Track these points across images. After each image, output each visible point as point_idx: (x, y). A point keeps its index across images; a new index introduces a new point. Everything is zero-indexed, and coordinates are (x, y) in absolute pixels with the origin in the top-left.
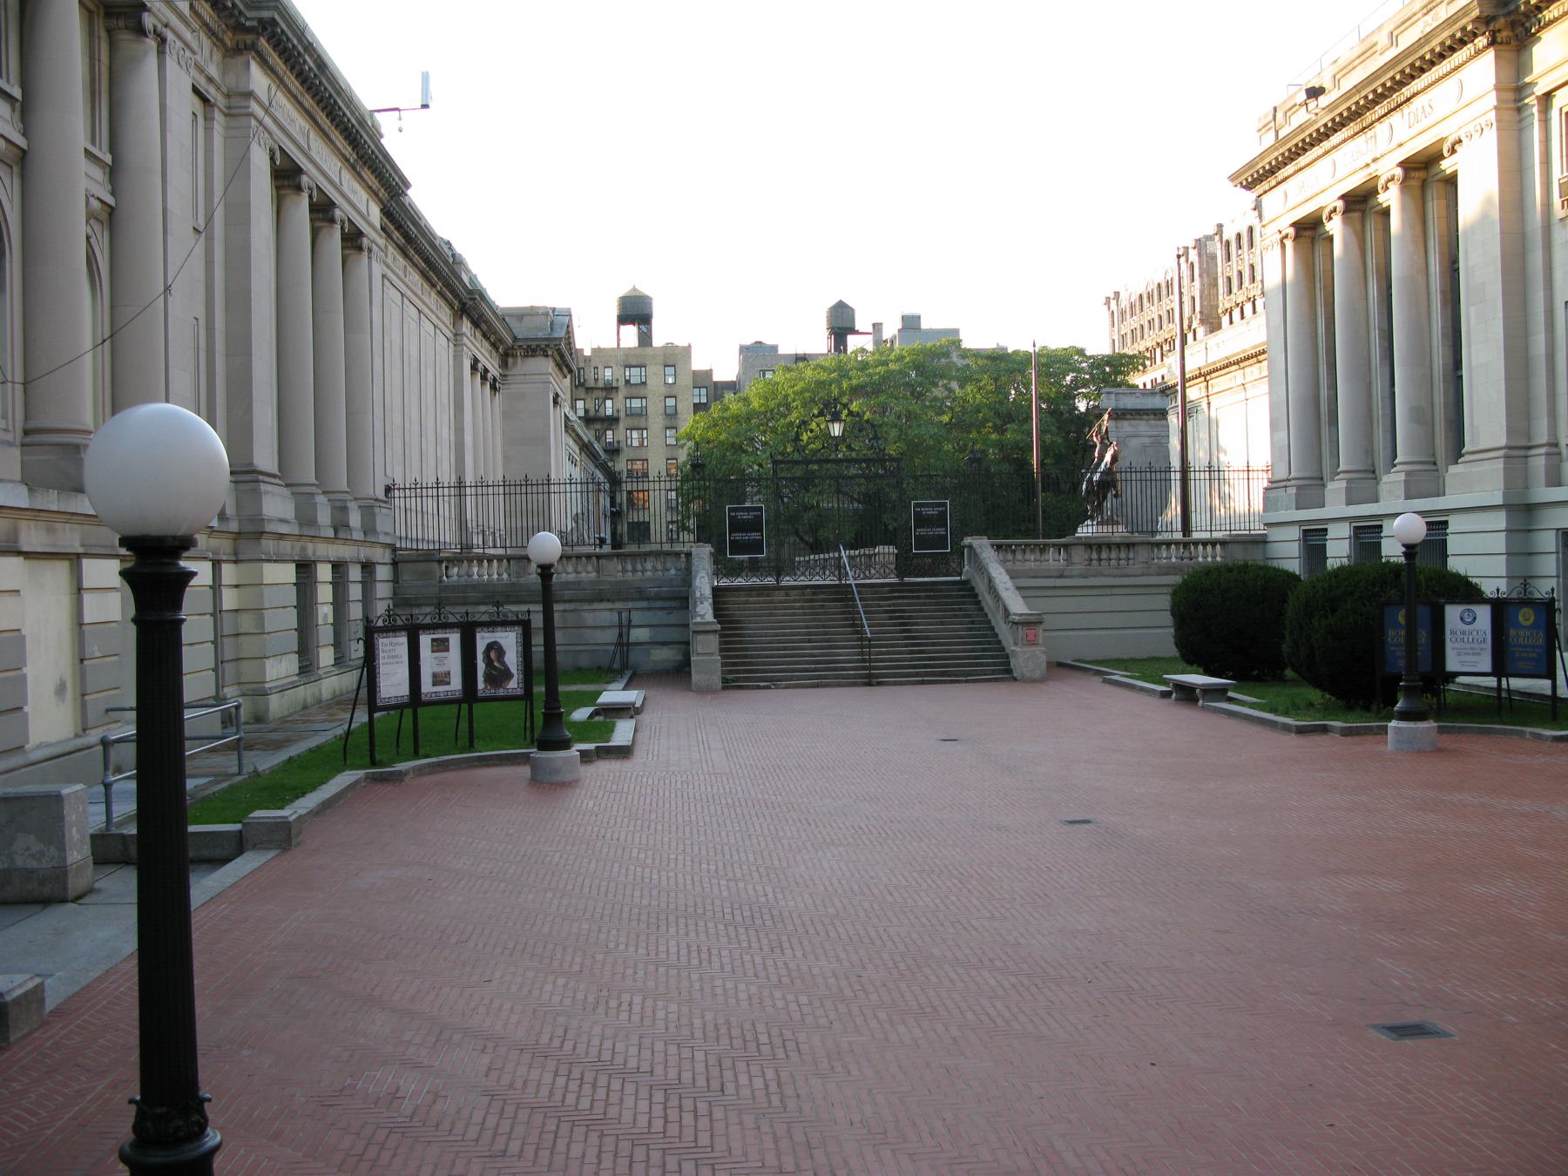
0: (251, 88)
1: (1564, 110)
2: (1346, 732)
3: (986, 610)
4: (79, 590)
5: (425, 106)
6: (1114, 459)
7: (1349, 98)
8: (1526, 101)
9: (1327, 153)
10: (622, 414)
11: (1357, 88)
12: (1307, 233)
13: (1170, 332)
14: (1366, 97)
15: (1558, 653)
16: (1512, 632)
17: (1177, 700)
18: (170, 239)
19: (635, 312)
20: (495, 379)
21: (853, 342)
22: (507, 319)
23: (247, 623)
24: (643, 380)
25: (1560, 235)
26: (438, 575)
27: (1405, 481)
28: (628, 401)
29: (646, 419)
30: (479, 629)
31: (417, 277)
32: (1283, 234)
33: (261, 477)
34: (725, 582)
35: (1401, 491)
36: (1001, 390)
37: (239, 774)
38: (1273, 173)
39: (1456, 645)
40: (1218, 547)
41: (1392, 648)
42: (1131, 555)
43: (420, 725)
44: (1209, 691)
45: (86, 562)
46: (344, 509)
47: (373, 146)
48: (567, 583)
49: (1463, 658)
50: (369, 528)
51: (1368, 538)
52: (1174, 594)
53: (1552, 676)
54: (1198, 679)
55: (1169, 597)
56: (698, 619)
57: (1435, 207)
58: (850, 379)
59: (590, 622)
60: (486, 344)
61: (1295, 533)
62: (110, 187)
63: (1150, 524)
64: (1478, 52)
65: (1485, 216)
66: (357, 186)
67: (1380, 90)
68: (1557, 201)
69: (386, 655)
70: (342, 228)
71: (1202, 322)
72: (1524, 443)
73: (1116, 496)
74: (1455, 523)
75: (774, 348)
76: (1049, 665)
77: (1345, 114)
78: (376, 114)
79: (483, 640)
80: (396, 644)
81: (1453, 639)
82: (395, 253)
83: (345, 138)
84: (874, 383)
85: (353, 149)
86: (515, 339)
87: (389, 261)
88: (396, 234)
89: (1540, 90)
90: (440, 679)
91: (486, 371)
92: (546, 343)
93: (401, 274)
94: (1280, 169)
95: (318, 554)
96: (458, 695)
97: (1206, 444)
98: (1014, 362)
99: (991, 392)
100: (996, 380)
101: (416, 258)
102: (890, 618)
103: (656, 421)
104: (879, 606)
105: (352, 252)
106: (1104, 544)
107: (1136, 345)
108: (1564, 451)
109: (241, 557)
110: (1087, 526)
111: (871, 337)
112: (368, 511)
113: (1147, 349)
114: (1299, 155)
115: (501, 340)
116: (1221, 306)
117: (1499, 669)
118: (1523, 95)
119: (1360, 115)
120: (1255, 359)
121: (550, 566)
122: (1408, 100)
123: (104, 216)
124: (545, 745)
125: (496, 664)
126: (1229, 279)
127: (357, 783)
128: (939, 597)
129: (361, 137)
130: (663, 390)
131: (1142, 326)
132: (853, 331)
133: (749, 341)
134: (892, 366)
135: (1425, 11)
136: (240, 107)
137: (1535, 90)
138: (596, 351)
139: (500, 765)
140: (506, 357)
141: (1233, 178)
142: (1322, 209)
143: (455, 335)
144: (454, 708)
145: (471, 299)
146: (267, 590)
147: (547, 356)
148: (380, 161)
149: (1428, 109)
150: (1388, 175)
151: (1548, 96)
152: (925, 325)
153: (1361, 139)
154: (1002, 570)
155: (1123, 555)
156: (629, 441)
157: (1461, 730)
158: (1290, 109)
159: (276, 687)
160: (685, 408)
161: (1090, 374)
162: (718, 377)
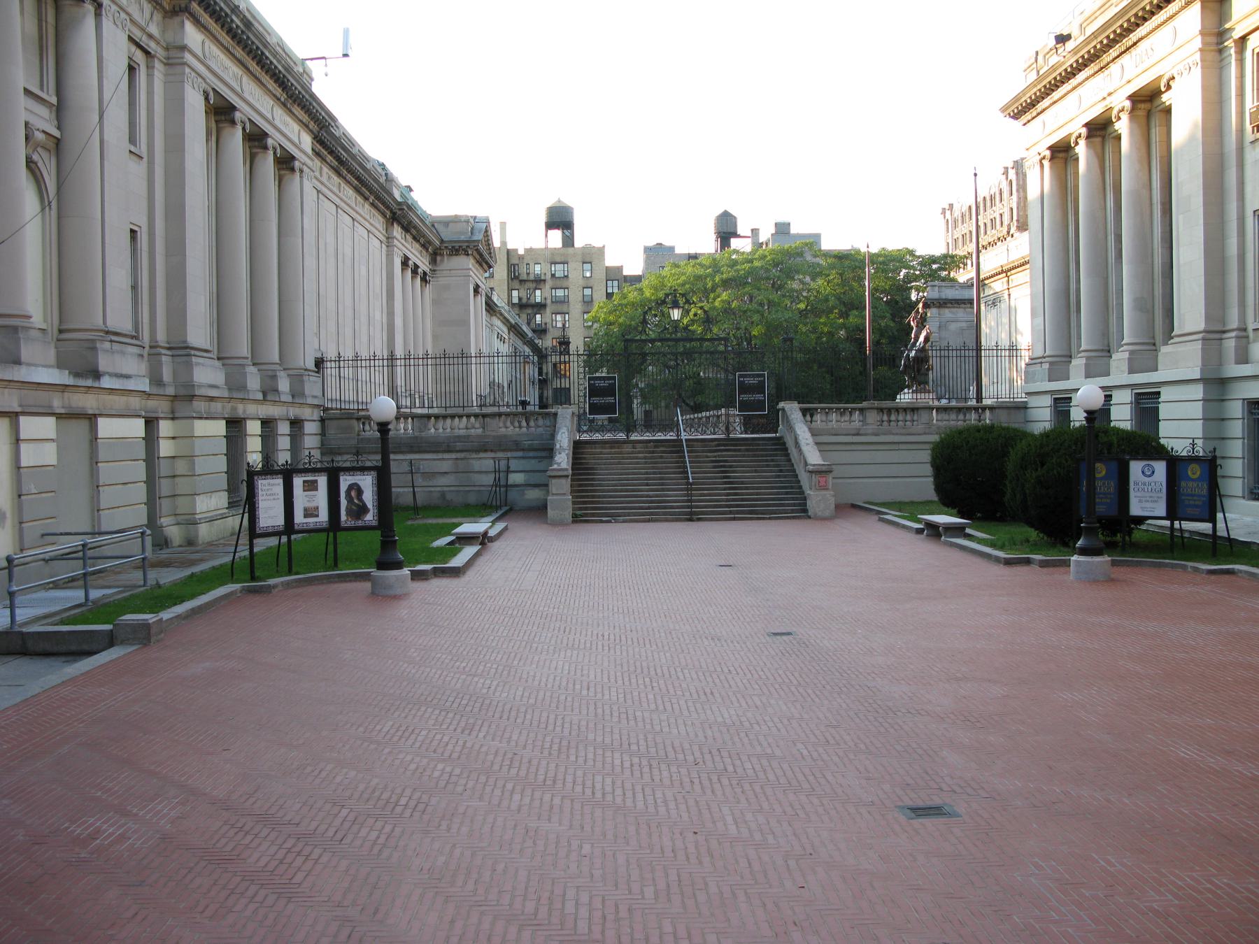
0: (185, 42)
1: (1256, 51)
2: (1043, 564)
3: (793, 461)
4: (17, 441)
5: (346, 55)
6: (927, 339)
7: (1089, 43)
8: (1226, 44)
9: (1074, 88)
10: (549, 302)
11: (1095, 35)
12: (1061, 155)
14: (1101, 42)
15: (1218, 500)
16: (1183, 484)
17: (927, 535)
18: (106, 163)
19: (560, 220)
20: (425, 273)
21: (735, 243)
22: (436, 225)
23: (181, 467)
24: (566, 274)
25: (1252, 155)
26: (357, 429)
27: (1129, 359)
28: (553, 291)
29: (568, 307)
30: (342, 473)
31: (351, 192)
32: (1042, 156)
33: (193, 352)
34: (585, 437)
35: (1125, 367)
37: (144, 586)
38: (1034, 106)
39: (1139, 494)
41: (1183, 498)
42: (915, 418)
43: (339, 551)
45: (22, 419)
46: (274, 377)
47: (299, 88)
48: (459, 437)
49: (1144, 505)
50: (297, 394)
51: (1148, 404)
52: (933, 450)
53: (1213, 520)
54: (942, 519)
55: (929, 452)
56: (555, 466)
57: (1156, 133)
58: (722, 274)
59: (477, 469)
60: (418, 246)
61: (1047, 401)
62: (56, 122)
63: (963, 393)
65: (1192, 138)
66: (289, 120)
67: (1112, 36)
68: (1248, 127)
69: (264, 493)
70: (275, 153)
72: (1221, 328)
74: (1166, 394)
75: (672, 249)
77: (1086, 56)
78: (307, 62)
79: (345, 481)
80: (273, 485)
81: (1136, 489)
82: (330, 173)
83: (275, 82)
84: (741, 277)
85: (283, 90)
86: (442, 241)
87: (324, 179)
88: (329, 158)
89: (1237, 34)
90: (309, 513)
91: (416, 267)
92: (466, 244)
93: (335, 189)
94: (1039, 102)
95: (248, 413)
96: (325, 525)
97: (1007, 327)
99: (838, 285)
100: (841, 275)
101: (349, 177)
102: (715, 467)
103: (576, 307)
104: (707, 457)
105: (287, 172)
106: (893, 408)
107: (965, 247)
108: (1251, 334)
109: (177, 415)
110: (904, 394)
111: (749, 240)
112: (297, 379)
114: (1053, 91)
115: (430, 243)
117: (1172, 514)
118: (1225, 39)
119: (1098, 57)
121: (387, 424)
122: (1135, 44)
123: (51, 145)
124: (383, 565)
125: (356, 501)
127: (232, 593)
128: (757, 450)
129: (288, 80)
130: (581, 282)
132: (736, 235)
133: (651, 243)
134: (756, 264)
136: (178, 58)
138: (529, 251)
139: (355, 581)
140: (435, 256)
141: (1003, 110)
142: (1070, 135)
143: (388, 238)
144: (324, 535)
145: (400, 209)
146: (197, 442)
147: (468, 255)
148: (307, 100)
150: (1120, 107)
151: (1244, 39)
152: (793, 230)
153: (1100, 76)
155: (908, 417)
156: (554, 323)
157: (1139, 564)
158: (1048, 53)
159: (205, 518)
160: (600, 297)
161: (920, 270)
162: (627, 272)
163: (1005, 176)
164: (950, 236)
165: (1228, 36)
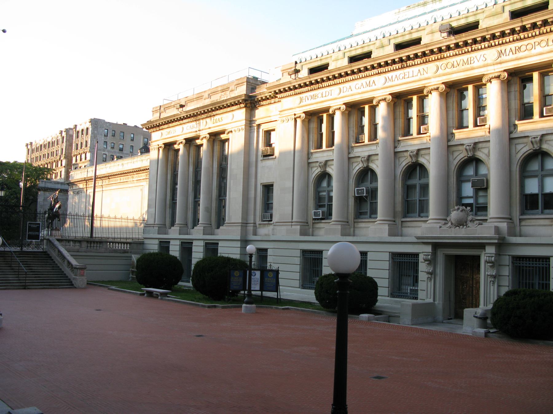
2: (223, 307)
3: (56, 262)
6: (59, 207)
8: (253, 125)
12: (168, 147)
13: (51, 159)
16: (266, 279)
32: (160, 146)
36: (20, 179)
40: (128, 244)
42: (101, 246)
44: (162, 294)
64: (241, 108)
71: (65, 158)
72: (245, 222)
73: (59, 221)
74: (221, 244)
76: (87, 284)
97: (85, 203)
98: (9, 166)
108: (258, 226)
113: (42, 165)
116: (73, 153)
118: (252, 123)
120: (108, 178)
126: (77, 144)
131: (40, 156)
135: (222, 91)
137: (256, 122)
149: (220, 120)
153: (194, 123)
154: (64, 249)
155: (98, 245)
163: (60, 135)
164: (30, 156)
165: (254, 122)
